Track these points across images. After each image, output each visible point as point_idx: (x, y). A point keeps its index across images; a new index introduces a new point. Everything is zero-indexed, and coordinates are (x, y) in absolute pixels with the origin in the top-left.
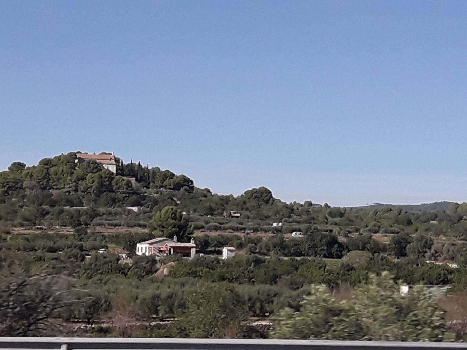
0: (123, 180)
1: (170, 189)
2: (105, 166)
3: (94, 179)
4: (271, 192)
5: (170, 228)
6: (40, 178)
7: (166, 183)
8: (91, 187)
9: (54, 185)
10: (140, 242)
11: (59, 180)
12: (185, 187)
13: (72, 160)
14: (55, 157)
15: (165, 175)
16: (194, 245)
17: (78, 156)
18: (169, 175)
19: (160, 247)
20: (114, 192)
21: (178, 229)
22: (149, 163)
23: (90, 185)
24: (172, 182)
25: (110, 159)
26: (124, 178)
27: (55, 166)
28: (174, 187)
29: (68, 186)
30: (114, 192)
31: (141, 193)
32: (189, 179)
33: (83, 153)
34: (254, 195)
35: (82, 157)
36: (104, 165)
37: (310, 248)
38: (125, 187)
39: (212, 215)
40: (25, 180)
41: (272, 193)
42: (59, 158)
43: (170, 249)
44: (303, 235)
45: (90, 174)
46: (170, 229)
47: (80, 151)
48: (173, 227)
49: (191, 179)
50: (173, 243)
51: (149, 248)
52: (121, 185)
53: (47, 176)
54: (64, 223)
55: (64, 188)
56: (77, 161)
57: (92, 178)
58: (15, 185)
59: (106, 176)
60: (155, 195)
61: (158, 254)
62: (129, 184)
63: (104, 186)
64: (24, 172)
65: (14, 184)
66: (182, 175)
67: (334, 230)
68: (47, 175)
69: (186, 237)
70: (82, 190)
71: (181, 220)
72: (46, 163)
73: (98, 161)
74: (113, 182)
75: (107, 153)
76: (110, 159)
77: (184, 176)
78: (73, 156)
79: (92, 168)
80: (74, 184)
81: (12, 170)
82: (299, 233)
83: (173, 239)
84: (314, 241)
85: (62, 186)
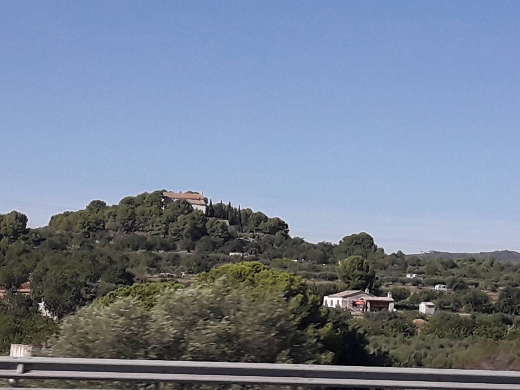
0: (218, 222)
1: (265, 233)
2: (195, 207)
3: (187, 220)
4: (372, 239)
5: (356, 279)
6: (125, 218)
7: (260, 227)
8: (184, 229)
9: (140, 227)
10: (327, 295)
11: (146, 220)
12: (280, 232)
13: (159, 199)
14: (139, 196)
15: (259, 217)
16: (392, 300)
17: (165, 194)
18: (261, 218)
19: (355, 300)
20: (208, 235)
21: (365, 281)
22: (239, 204)
23: (181, 227)
24: (268, 226)
25: (199, 199)
26: (219, 220)
27: (139, 205)
28: (270, 231)
29: (158, 228)
30: (208, 235)
31: (237, 237)
32: (284, 222)
33: (168, 191)
34: (354, 241)
35: (168, 196)
36: (193, 206)
37: (506, 305)
38: (221, 230)
39: (327, 263)
40: (107, 221)
41: (374, 240)
42: (143, 197)
43: (367, 303)
44: (448, 288)
45: (182, 215)
46: (357, 281)
47: (165, 189)
48: (359, 279)
49: (286, 222)
50: (366, 297)
51: (342, 301)
52: (215, 227)
53: (132, 217)
54: (190, 270)
55: (152, 230)
56: (163, 200)
57: (184, 219)
58: (97, 225)
59: (200, 217)
60: (252, 239)
61: (352, 309)
62: (224, 226)
63: (197, 228)
64: (107, 212)
65: (95, 225)
66: (277, 218)
67: (480, 283)
68: (133, 216)
69: (373, 290)
70: (173, 232)
71: (368, 271)
72: (129, 201)
73: (188, 200)
74: (208, 225)
75: (193, 191)
76: (199, 199)
77: (279, 219)
78: (160, 194)
79: (182, 208)
80: (164, 225)
81: (91, 209)
82: (443, 286)
83: (364, 291)
84: (510, 297)
85: (150, 227)
